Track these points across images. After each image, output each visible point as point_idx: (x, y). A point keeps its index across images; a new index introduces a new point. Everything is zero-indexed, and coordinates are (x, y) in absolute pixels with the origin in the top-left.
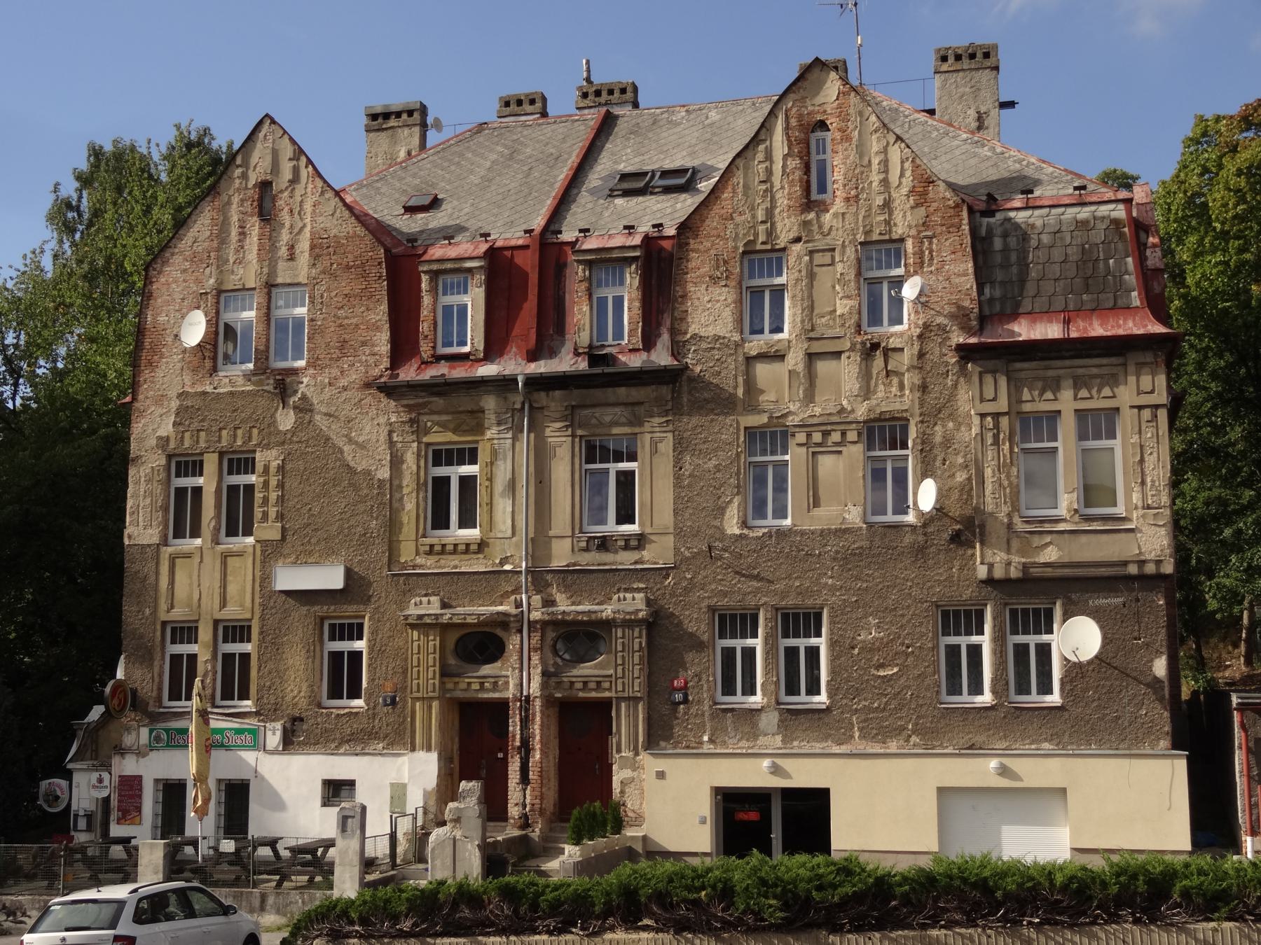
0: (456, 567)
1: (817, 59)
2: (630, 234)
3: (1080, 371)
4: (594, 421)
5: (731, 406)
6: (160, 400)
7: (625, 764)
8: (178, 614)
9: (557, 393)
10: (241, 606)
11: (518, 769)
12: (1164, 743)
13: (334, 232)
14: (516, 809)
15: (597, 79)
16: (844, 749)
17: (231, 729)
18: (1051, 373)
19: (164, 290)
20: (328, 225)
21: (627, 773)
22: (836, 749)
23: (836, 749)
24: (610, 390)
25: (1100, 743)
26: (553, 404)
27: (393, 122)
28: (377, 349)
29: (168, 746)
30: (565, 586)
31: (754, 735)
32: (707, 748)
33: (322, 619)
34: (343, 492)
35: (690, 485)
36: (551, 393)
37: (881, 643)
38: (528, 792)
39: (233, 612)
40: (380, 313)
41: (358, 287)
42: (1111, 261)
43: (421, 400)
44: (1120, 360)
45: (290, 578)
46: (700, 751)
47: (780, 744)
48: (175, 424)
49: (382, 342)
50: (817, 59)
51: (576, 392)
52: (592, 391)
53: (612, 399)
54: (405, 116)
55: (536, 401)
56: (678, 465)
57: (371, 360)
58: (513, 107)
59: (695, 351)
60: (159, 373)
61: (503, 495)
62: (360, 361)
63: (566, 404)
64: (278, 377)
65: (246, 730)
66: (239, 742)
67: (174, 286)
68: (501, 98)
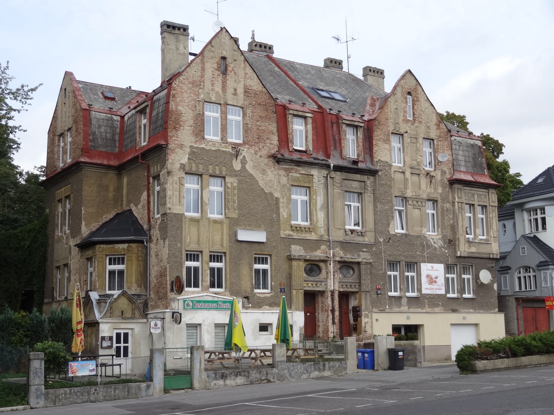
0: (304, 237)
1: (271, 48)
2: (303, 106)
3: (479, 192)
4: (349, 186)
5: (391, 188)
6: (181, 146)
7: (367, 316)
8: (193, 247)
9: (338, 173)
10: (222, 246)
11: (332, 318)
12: (497, 310)
13: (254, 88)
14: (331, 334)
15: (258, 39)
16: (424, 311)
17: (221, 301)
18: (472, 192)
19: (180, 94)
20: (252, 84)
21: (366, 320)
22: (422, 311)
23: (422, 311)
24: (355, 175)
25: (484, 310)
26: (337, 177)
27: (177, 31)
28: (272, 142)
29: (193, 308)
30: (343, 248)
31: (400, 305)
32: (388, 310)
33: (270, 255)
34: (262, 201)
35: (380, 215)
36: (336, 172)
37: (94, 207)
38: (335, 327)
39: (217, 248)
40: (273, 127)
41: (264, 114)
42: (480, 159)
43: (291, 167)
44: (487, 191)
45: (244, 235)
46: (385, 312)
47: (407, 310)
48: (189, 159)
49: (275, 139)
50: (271, 48)
51: (344, 174)
52: (349, 174)
53: (356, 179)
54: (182, 30)
55: (331, 175)
56: (375, 206)
57: (271, 146)
58: (263, 48)
59: (379, 165)
60: (179, 133)
61: (321, 210)
62: (266, 146)
63: (341, 178)
64: (233, 146)
65: (227, 301)
66: (225, 307)
67: (185, 94)
68: (273, 46)
